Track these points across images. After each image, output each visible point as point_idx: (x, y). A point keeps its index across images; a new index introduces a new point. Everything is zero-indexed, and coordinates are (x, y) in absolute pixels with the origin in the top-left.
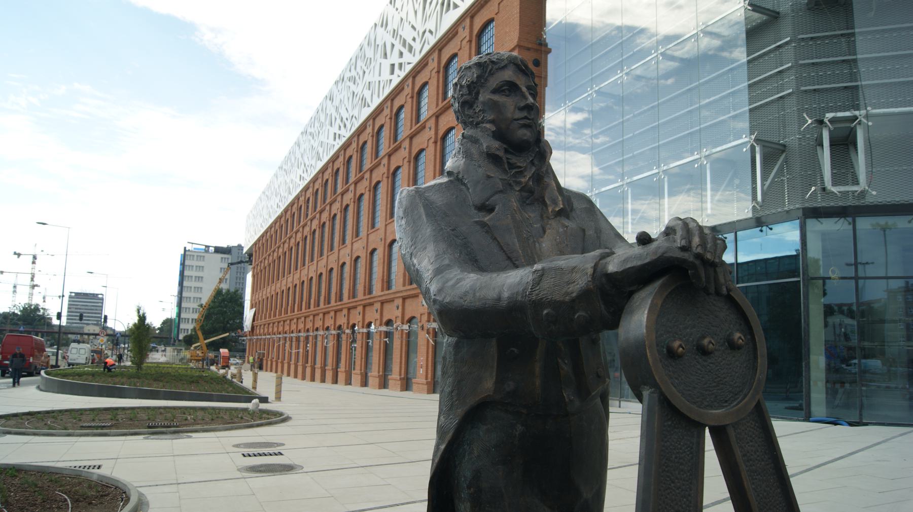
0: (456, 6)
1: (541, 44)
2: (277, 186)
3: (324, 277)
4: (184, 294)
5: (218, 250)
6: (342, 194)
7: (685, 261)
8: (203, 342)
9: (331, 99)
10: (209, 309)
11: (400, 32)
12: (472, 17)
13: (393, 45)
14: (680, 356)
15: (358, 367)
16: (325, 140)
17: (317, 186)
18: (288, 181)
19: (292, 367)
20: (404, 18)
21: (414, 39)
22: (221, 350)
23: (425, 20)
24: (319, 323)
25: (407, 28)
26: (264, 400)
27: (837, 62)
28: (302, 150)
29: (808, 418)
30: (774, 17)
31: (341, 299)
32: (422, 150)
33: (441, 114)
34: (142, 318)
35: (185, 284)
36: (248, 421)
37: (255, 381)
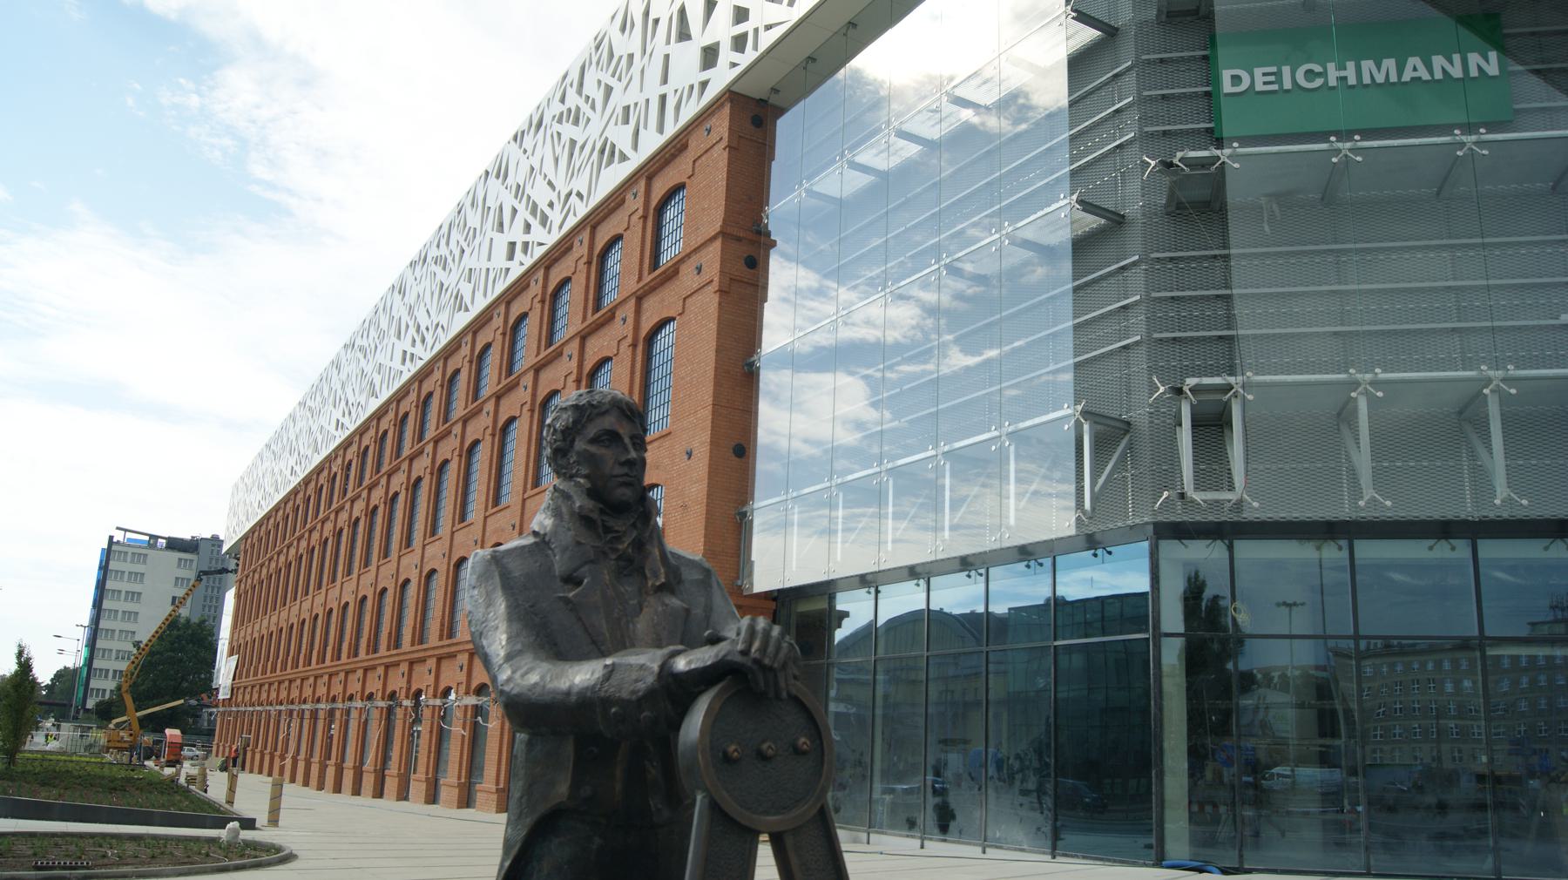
0: (624, 158)
1: (759, 233)
2: (293, 437)
3: (369, 603)
4: (103, 624)
5: (174, 544)
6: (412, 459)
7: (743, 665)
8: (134, 715)
9: (402, 292)
10: (151, 654)
11: (528, 190)
12: (650, 179)
13: (515, 211)
14: (736, 761)
15: (421, 768)
16: (388, 363)
17: (365, 442)
18: (314, 428)
19: (301, 765)
20: (537, 167)
21: (551, 205)
22: (168, 731)
23: (572, 174)
24: (354, 687)
25: (541, 183)
26: (249, 824)
27: (1208, 298)
28: (343, 376)
29: (1160, 861)
30: (1117, 221)
31: (397, 645)
34: (25, 666)
35: (106, 604)
36: (218, 860)
37: (232, 790)
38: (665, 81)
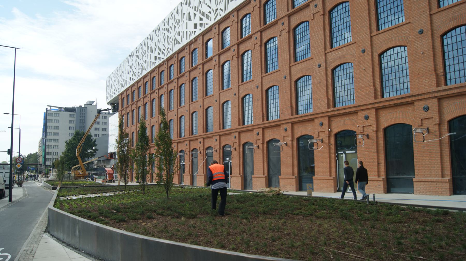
5: (67, 110)
11: (200, 8)
16: (125, 79)
32: (162, 95)
33: (291, 15)
38: (187, 29)
